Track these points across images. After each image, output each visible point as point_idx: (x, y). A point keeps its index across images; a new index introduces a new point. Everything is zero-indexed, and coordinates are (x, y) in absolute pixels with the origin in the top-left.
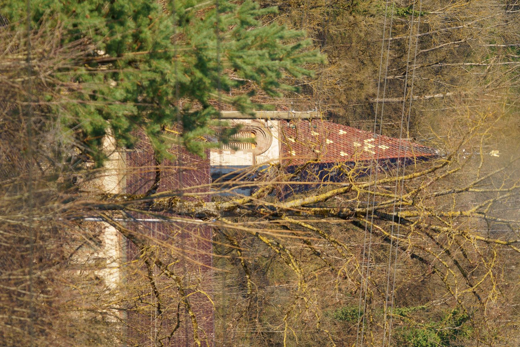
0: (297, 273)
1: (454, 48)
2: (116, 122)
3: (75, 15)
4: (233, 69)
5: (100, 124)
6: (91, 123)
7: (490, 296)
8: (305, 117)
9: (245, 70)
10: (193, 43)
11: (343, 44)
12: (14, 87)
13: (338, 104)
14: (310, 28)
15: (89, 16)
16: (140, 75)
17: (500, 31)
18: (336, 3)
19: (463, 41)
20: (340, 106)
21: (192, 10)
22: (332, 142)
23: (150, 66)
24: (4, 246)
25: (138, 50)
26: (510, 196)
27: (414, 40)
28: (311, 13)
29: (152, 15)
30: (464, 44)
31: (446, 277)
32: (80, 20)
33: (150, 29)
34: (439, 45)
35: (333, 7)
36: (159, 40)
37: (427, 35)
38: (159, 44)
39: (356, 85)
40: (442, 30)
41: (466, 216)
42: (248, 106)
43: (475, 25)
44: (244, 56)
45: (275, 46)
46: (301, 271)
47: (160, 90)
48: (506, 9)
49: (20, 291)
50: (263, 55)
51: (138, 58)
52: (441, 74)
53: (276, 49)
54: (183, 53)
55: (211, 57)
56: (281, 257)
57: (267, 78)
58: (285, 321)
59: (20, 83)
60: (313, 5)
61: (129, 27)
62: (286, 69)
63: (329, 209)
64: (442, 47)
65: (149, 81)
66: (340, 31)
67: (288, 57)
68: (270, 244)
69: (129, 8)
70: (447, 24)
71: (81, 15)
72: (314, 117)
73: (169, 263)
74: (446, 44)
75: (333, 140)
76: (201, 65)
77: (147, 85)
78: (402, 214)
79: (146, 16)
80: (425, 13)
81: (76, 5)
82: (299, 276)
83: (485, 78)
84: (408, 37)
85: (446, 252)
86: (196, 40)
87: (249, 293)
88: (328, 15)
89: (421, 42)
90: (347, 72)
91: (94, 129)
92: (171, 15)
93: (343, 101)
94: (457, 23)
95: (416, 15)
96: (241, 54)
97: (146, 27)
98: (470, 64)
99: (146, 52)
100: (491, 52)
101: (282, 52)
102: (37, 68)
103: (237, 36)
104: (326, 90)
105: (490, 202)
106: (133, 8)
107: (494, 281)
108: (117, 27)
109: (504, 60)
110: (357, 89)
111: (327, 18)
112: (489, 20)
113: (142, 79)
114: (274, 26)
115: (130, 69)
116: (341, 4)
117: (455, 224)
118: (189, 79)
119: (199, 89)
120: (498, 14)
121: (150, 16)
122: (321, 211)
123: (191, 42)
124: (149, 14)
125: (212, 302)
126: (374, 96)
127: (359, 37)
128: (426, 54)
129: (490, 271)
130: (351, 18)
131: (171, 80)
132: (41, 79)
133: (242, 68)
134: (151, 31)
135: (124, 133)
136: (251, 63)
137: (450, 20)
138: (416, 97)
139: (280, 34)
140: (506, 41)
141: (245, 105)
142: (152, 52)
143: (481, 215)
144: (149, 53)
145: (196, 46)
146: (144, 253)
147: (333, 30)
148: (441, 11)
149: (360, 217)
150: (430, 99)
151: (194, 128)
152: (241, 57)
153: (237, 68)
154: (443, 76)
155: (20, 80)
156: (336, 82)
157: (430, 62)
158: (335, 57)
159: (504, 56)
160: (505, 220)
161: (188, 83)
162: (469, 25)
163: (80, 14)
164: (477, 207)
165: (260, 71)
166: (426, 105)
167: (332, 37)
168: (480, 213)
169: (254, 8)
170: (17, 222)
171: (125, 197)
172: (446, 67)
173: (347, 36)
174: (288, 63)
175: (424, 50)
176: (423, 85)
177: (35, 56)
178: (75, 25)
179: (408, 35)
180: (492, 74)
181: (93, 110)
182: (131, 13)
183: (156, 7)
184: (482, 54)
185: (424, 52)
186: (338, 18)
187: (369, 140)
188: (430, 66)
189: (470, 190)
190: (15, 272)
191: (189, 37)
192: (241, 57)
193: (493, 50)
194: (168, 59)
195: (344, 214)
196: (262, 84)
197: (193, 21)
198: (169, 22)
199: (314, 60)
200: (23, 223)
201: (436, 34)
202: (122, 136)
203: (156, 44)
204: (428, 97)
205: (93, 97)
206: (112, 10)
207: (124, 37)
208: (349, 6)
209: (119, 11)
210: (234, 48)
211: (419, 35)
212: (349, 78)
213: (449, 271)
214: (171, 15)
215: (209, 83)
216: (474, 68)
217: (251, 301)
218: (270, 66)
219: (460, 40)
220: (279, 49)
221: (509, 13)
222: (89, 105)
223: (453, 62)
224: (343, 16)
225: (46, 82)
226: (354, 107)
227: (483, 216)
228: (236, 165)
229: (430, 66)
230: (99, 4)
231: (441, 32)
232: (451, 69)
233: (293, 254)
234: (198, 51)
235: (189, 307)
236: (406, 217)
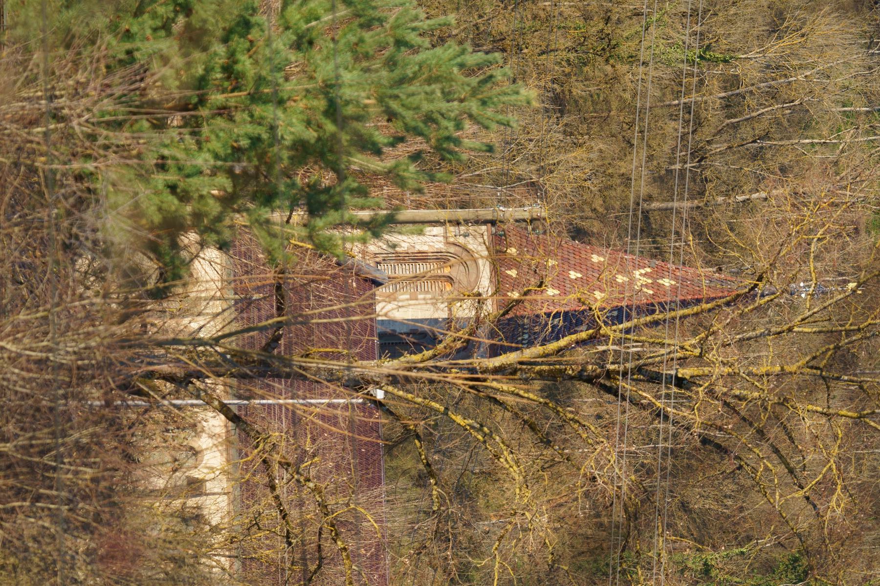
0: (513, 474)
1: (783, 115)
2: (199, 206)
3: (128, 35)
4: (386, 118)
5: (173, 208)
6: (160, 209)
7: (833, 504)
8: (521, 217)
9: (404, 118)
10: (319, 77)
11: (595, 112)
12: (31, 142)
13: (590, 214)
14: (539, 87)
15: (151, 37)
16: (236, 130)
17: (858, 84)
18: (581, 44)
19: (797, 103)
20: (594, 216)
21: (317, 25)
22: (579, 275)
23: (252, 116)
24: (22, 393)
25: (232, 91)
26: (861, 339)
27: (714, 103)
28: (540, 62)
29: (254, 34)
30: (798, 107)
31: (759, 474)
32: (138, 44)
33: (250, 57)
34: (758, 110)
35: (576, 51)
36: (264, 73)
37: (737, 95)
38: (265, 79)
39: (619, 181)
40: (762, 85)
41: (791, 373)
42: (412, 176)
43: (817, 76)
44: (401, 95)
45: (452, 80)
46: (520, 470)
47: (270, 154)
48: (869, 48)
49: (46, 462)
50: (433, 92)
51: (232, 103)
52: (762, 159)
53: (454, 84)
54: (304, 93)
55: (348, 98)
56: (487, 448)
57: (441, 131)
58: (496, 552)
59: (40, 135)
60: (543, 48)
61: (216, 54)
62: (471, 116)
63: (564, 367)
64: (762, 114)
65: (251, 138)
66: (590, 91)
67: (474, 97)
68: (468, 428)
69: (216, 26)
70: (770, 74)
71: (138, 35)
72: (535, 216)
73: (302, 462)
74: (769, 109)
75: (581, 272)
76: (332, 111)
77: (247, 146)
78: (685, 372)
79: (243, 36)
80: (731, 57)
81: (131, 20)
82: (517, 478)
83: (836, 163)
84: (705, 98)
85: (757, 431)
86: (325, 71)
87: (435, 508)
88: (569, 65)
89: (727, 106)
90: (603, 159)
91: (164, 218)
92: (283, 32)
93: (598, 208)
94: (787, 72)
95: (716, 61)
96: (396, 92)
97: (244, 54)
98: (810, 141)
99: (245, 93)
100: (846, 119)
101: (463, 89)
102: (66, 111)
103: (391, 63)
104: (569, 190)
105: (828, 349)
106: (221, 25)
107: (839, 478)
108: (197, 55)
109: (867, 133)
110: (622, 188)
111: (567, 70)
112: (840, 67)
113: (238, 136)
114: (450, 47)
115: (220, 122)
116: (590, 46)
117: (772, 386)
118: (315, 134)
119: (331, 151)
120: (855, 56)
121: (250, 37)
122: (550, 371)
123: (315, 75)
124: (248, 33)
125: (375, 525)
126: (649, 198)
127: (621, 99)
128: (735, 127)
129: (832, 461)
130: (609, 68)
131: (285, 137)
132: (73, 128)
133: (401, 115)
134: (251, 60)
135: (214, 225)
136: (414, 106)
137: (773, 68)
138: (720, 199)
139: (459, 60)
140: (870, 102)
141: (406, 174)
142: (255, 93)
143: (815, 371)
144: (249, 94)
145: (324, 81)
146: (261, 446)
147: (578, 89)
148: (759, 53)
149: (615, 379)
150: (744, 201)
151: (325, 212)
152: (396, 97)
153: (391, 116)
154: (764, 163)
155: (39, 129)
156: (585, 177)
157: (743, 140)
158: (582, 135)
159: (867, 126)
160: (855, 379)
161: (313, 141)
162: (806, 76)
163: (136, 34)
164: (808, 358)
165: (429, 119)
166: (738, 212)
167: (576, 102)
168: (812, 368)
169: (416, 18)
170: (40, 354)
171: (229, 356)
172: (770, 147)
173: (601, 99)
174: (474, 106)
175: (733, 120)
176: (732, 178)
177: (63, 92)
178: (129, 52)
179: (704, 95)
180: (847, 157)
181: (160, 186)
182: (219, 33)
183: (261, 22)
184: (830, 123)
185: (732, 123)
186: (585, 69)
187: (643, 271)
188: (743, 145)
189: (796, 329)
190: (38, 434)
191: (312, 68)
192: (396, 97)
193: (848, 117)
194: (281, 102)
195: (588, 376)
196: (433, 140)
197: (319, 42)
198: (281, 44)
199: (516, 101)
200: (50, 355)
201: (751, 92)
202: (210, 228)
203: (260, 80)
204: (740, 198)
205: (162, 167)
206: (188, 27)
207: (208, 70)
208: (603, 49)
209: (201, 29)
210: (385, 82)
211: (723, 95)
212: (608, 168)
213: (764, 464)
214: (283, 32)
215: (347, 141)
216: (817, 148)
217: (439, 522)
218: (444, 111)
219: (793, 101)
220: (459, 83)
221: (873, 54)
222: (154, 179)
223: (781, 139)
224: (594, 65)
225: (82, 132)
226: (616, 217)
227: (819, 372)
228: (420, 317)
229: (743, 145)
230: (168, 18)
231: (759, 88)
232: (778, 149)
233: (507, 442)
234: (328, 89)
235: (336, 534)
236: (692, 377)
